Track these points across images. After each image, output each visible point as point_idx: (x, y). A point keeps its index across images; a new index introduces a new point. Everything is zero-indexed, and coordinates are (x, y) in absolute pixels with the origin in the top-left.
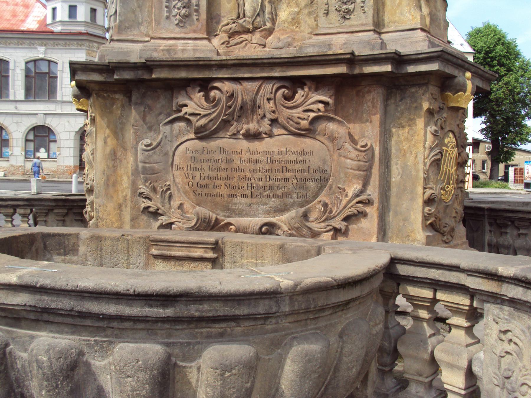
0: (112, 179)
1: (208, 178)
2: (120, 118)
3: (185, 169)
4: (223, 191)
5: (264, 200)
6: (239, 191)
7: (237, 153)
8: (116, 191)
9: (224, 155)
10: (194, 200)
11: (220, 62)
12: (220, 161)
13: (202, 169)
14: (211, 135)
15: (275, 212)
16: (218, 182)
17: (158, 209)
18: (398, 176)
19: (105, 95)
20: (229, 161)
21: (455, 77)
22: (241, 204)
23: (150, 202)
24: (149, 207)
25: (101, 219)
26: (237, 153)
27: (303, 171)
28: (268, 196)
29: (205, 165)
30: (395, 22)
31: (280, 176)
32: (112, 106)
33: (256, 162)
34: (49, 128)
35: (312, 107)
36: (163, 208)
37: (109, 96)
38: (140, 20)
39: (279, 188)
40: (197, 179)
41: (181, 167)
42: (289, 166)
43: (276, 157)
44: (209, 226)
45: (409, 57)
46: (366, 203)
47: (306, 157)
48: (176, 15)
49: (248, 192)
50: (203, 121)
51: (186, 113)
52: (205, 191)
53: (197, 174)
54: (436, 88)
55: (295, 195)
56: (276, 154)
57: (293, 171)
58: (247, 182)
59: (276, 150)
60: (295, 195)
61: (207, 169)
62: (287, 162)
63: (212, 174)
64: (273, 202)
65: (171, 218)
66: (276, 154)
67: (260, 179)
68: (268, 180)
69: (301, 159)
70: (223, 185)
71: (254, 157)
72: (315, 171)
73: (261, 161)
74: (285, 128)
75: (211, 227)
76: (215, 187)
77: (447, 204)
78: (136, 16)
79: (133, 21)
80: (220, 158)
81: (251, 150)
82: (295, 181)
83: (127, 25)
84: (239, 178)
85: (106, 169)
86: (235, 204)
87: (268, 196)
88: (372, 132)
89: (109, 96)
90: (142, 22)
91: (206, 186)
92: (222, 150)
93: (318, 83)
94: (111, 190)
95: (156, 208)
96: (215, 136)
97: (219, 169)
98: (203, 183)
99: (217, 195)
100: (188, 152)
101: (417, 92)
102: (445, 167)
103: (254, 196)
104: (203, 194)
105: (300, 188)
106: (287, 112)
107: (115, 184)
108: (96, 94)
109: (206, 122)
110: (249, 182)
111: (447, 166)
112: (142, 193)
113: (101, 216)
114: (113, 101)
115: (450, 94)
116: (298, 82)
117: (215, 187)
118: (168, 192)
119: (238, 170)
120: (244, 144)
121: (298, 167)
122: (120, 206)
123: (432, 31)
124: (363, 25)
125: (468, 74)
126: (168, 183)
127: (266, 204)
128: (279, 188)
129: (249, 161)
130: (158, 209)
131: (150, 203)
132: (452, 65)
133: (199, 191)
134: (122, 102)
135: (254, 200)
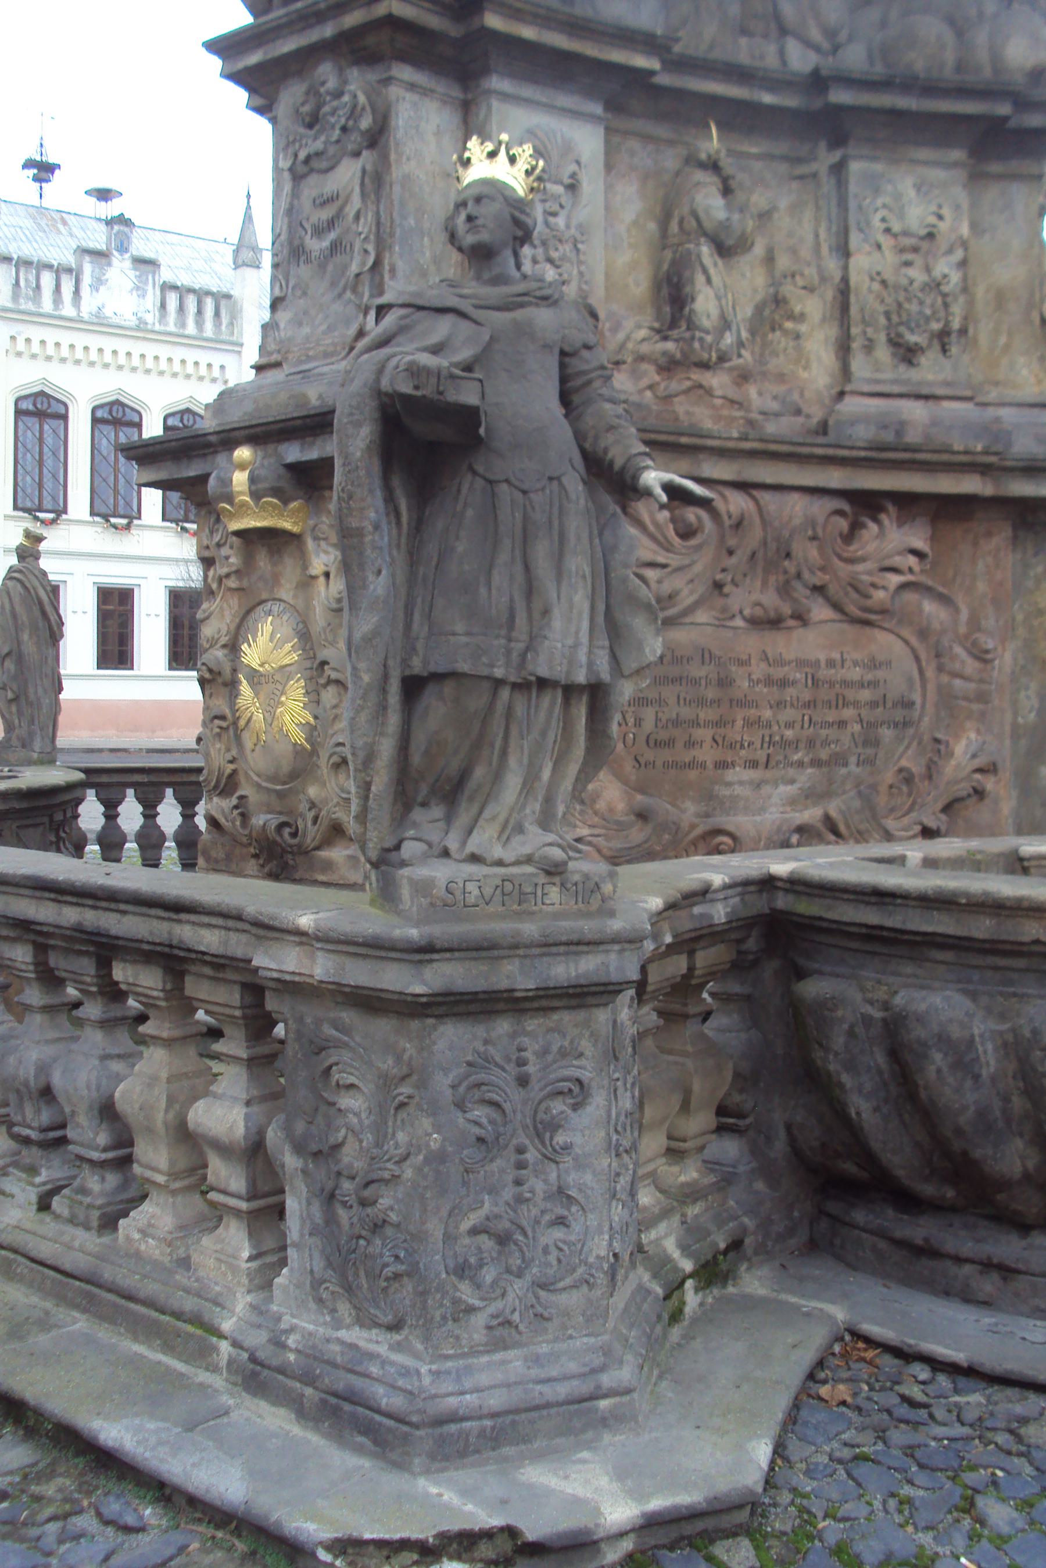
1: (677, 723)
4: (707, 754)
5: (791, 772)
6: (743, 753)
7: (742, 663)
9: (712, 667)
11: (263, 428)
12: (703, 682)
13: (661, 702)
15: (807, 797)
16: (699, 733)
18: (1030, 712)
20: (725, 682)
22: (741, 783)
26: (742, 663)
27: (874, 704)
28: (800, 764)
29: (669, 693)
30: (997, 384)
31: (831, 716)
33: (784, 683)
35: (897, 561)
39: (826, 743)
40: (648, 725)
42: (850, 694)
43: (824, 673)
47: (880, 674)
49: (761, 756)
52: (666, 755)
53: (649, 714)
55: (853, 760)
56: (823, 664)
57: (856, 704)
58: (761, 732)
59: (822, 657)
60: (853, 760)
61: (672, 700)
62: (846, 683)
63: (686, 712)
64: (807, 776)
65: (575, 826)
66: (823, 664)
67: (789, 725)
68: (806, 725)
69: (869, 677)
71: (779, 673)
72: (895, 705)
73: (794, 683)
74: (837, 607)
81: (770, 655)
82: (857, 727)
84: (749, 723)
86: (729, 784)
87: (800, 764)
91: (670, 743)
92: (707, 656)
93: (907, 503)
97: (701, 702)
98: (663, 735)
99: (691, 765)
103: (772, 763)
104: (659, 764)
105: (866, 743)
106: (844, 570)
110: (767, 732)
116: (866, 504)
117: (690, 744)
119: (743, 703)
120: (751, 643)
121: (866, 695)
124: (947, 384)
127: (792, 782)
128: (826, 743)
129: (769, 681)
133: (649, 755)
135: (768, 774)
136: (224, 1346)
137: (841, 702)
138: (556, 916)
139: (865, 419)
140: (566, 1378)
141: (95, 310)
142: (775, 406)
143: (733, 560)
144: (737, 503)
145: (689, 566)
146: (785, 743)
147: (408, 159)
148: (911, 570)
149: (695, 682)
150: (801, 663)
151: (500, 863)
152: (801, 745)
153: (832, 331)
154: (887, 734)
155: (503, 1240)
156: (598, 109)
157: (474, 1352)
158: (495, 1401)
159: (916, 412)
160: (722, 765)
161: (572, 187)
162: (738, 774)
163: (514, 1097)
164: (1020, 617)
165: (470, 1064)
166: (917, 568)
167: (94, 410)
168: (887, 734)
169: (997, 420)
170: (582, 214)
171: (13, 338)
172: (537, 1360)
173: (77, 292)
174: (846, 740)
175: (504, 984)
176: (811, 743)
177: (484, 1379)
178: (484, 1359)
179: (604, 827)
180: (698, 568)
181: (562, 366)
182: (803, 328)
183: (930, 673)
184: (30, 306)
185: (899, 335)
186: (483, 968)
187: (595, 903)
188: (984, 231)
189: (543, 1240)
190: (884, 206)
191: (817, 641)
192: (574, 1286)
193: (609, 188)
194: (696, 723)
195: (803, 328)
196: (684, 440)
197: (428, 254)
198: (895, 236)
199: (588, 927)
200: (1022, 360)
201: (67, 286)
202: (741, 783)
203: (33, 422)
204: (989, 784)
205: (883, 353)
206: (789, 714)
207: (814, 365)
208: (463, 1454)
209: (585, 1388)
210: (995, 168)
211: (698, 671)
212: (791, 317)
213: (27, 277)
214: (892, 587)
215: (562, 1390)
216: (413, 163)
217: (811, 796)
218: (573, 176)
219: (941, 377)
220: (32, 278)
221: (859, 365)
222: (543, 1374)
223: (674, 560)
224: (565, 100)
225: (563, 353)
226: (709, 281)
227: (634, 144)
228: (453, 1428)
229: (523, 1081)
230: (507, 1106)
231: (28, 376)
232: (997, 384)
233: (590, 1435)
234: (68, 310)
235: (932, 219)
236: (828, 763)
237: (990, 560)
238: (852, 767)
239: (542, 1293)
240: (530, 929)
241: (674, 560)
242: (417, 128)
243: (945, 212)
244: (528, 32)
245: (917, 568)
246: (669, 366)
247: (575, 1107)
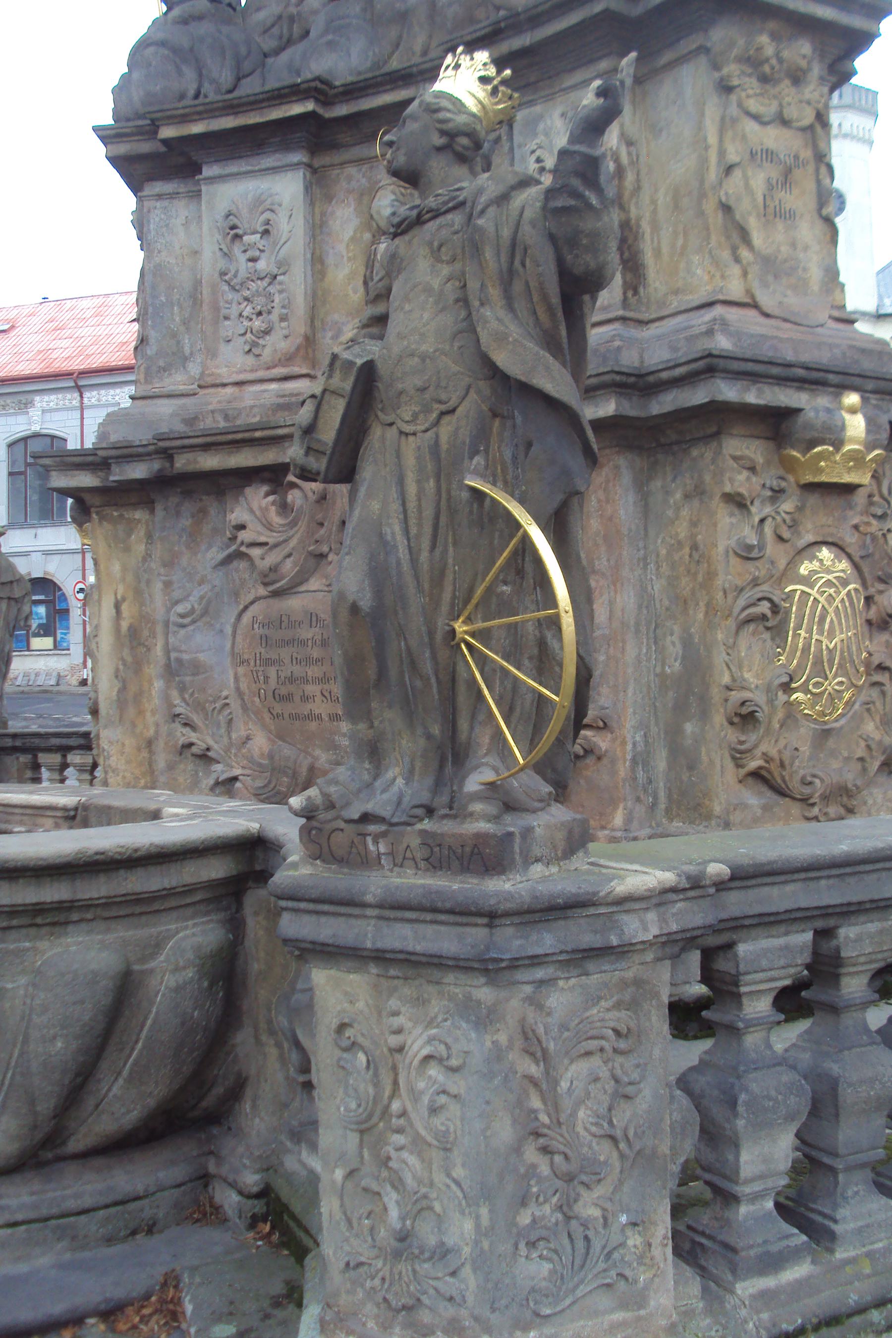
0: (133, 689)
1: (291, 680)
2: (144, 560)
3: (252, 663)
8: (141, 712)
9: (317, 629)
10: (273, 728)
14: (292, 588)
17: (208, 749)
18: (676, 660)
19: (115, 514)
21: (799, 411)
23: (193, 734)
24: (191, 745)
25: (113, 771)
29: (285, 653)
32: (129, 535)
34: (55, 584)
36: (216, 746)
37: (121, 516)
38: (187, 350)
41: (246, 657)
44: (297, 785)
45: (657, 375)
46: (598, 728)
48: (245, 333)
50: (272, 558)
51: (242, 543)
53: (272, 672)
54: (757, 442)
61: (287, 661)
63: (298, 670)
65: (232, 767)
70: (318, 694)
75: (300, 786)
76: (305, 698)
77: (826, 727)
78: (178, 342)
79: (174, 354)
80: (310, 636)
83: (161, 363)
85: (121, 667)
88: (608, 560)
89: (121, 516)
90: (191, 354)
92: (314, 619)
94: (131, 711)
95: (204, 746)
96: (303, 588)
97: (309, 661)
98: (283, 691)
99: (310, 717)
100: (256, 626)
101: (702, 456)
102: (802, 633)
104: (286, 716)
107: (138, 697)
108: (97, 513)
109: (279, 559)
111: (810, 631)
112: (179, 715)
113: (113, 764)
114: (131, 527)
115: (795, 453)
117: (305, 698)
118: (226, 712)
122: (150, 743)
123: (765, 300)
125: (852, 399)
126: (224, 693)
130: (208, 749)
131: (193, 737)
132: (778, 384)
133: (278, 708)
134: (147, 526)
145: (285, 541)
147: (159, 252)
149: (303, 643)
164: (664, 552)
179: (250, 768)
180: (293, 543)
188: (661, 130)
194: (305, 680)
196: (258, 434)
197: (177, 319)
200: (696, 259)
210: (668, 56)
211: (306, 633)
216: (164, 254)
224: (268, 161)
227: (352, 170)
232: (676, 292)
237: (601, 494)
242: (167, 225)
244: (197, 128)
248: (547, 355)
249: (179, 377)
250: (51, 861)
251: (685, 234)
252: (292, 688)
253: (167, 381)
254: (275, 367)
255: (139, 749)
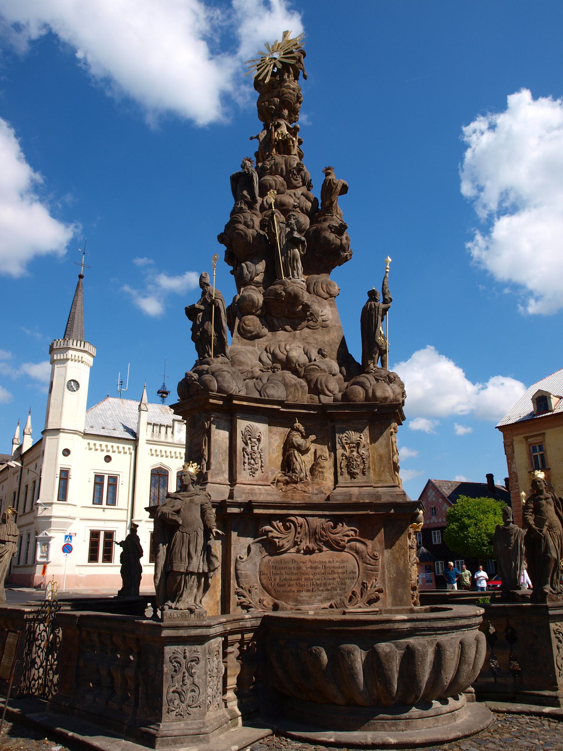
1: (285, 580)
3: (269, 574)
4: (295, 588)
7: (303, 563)
13: (281, 574)
16: (292, 582)
20: (299, 568)
22: (305, 596)
26: (303, 563)
27: (343, 573)
28: (323, 590)
33: (316, 568)
39: (329, 584)
40: (278, 581)
42: (336, 570)
43: (328, 565)
47: (345, 564)
49: (311, 588)
52: (283, 589)
53: (278, 577)
57: (338, 573)
60: (338, 589)
61: (284, 574)
63: (288, 577)
64: (325, 594)
69: (341, 565)
71: (314, 565)
82: (339, 580)
86: (302, 597)
87: (323, 590)
91: (284, 585)
97: (292, 574)
98: (282, 583)
99: (290, 591)
103: (314, 590)
104: (281, 591)
105: (342, 584)
110: (312, 582)
117: (290, 585)
121: (340, 570)
127: (321, 596)
128: (329, 584)
129: (311, 567)
135: (313, 594)
136: (125, 727)
137: (333, 572)
138: (193, 621)
139: (341, 494)
140: (194, 729)
141: (178, 439)
142: (315, 492)
143: (300, 535)
144: (301, 520)
146: (317, 585)
148: (352, 536)
149: (290, 568)
150: (320, 562)
151: (181, 609)
152: (322, 585)
153: (332, 470)
154: (348, 581)
155: (179, 694)
156: (266, 418)
157: (173, 721)
158: (176, 733)
159: (355, 491)
160: (299, 591)
161: (259, 440)
162: (304, 594)
163: (183, 661)
165: (173, 653)
166: (354, 535)
167: (152, 470)
168: (348, 581)
169: (378, 492)
170: (261, 446)
171: (151, 450)
172: (187, 724)
173: (173, 433)
174: (335, 583)
175: (180, 635)
176: (325, 584)
177: (174, 728)
178: (175, 723)
181: (201, 507)
182: (324, 470)
183: (360, 563)
184: (158, 439)
185: (351, 470)
186: (176, 631)
187: (202, 618)
189: (189, 695)
190: (346, 436)
191: (326, 556)
192: (196, 707)
193: (270, 438)
195: (324, 470)
198: (349, 444)
199: (198, 623)
201: (170, 430)
202: (305, 596)
203: (157, 477)
204: (381, 595)
205: (347, 476)
206: (317, 577)
207: (328, 480)
208: (167, 745)
209: (196, 732)
211: (291, 565)
212: (321, 467)
213: (156, 429)
214: (346, 541)
215: (191, 732)
217: (327, 599)
218: (259, 436)
219: (363, 481)
220: (158, 429)
221: (340, 478)
222: (188, 728)
223: (283, 536)
225: (201, 505)
226: (297, 460)
228: (165, 738)
229: (185, 657)
230: (181, 663)
231: (156, 462)
233: (198, 743)
234: (170, 440)
235: (359, 439)
236: (330, 590)
238: (339, 591)
239: (189, 708)
240: (186, 623)
241: (283, 536)
243: (363, 437)
245: (354, 535)
246: (287, 483)
247: (197, 664)
248: (220, 582)
249: (221, 478)
250: (78, 592)
251: (384, 467)
252: (284, 582)
253: (218, 478)
254: (259, 480)
255: (214, 605)
